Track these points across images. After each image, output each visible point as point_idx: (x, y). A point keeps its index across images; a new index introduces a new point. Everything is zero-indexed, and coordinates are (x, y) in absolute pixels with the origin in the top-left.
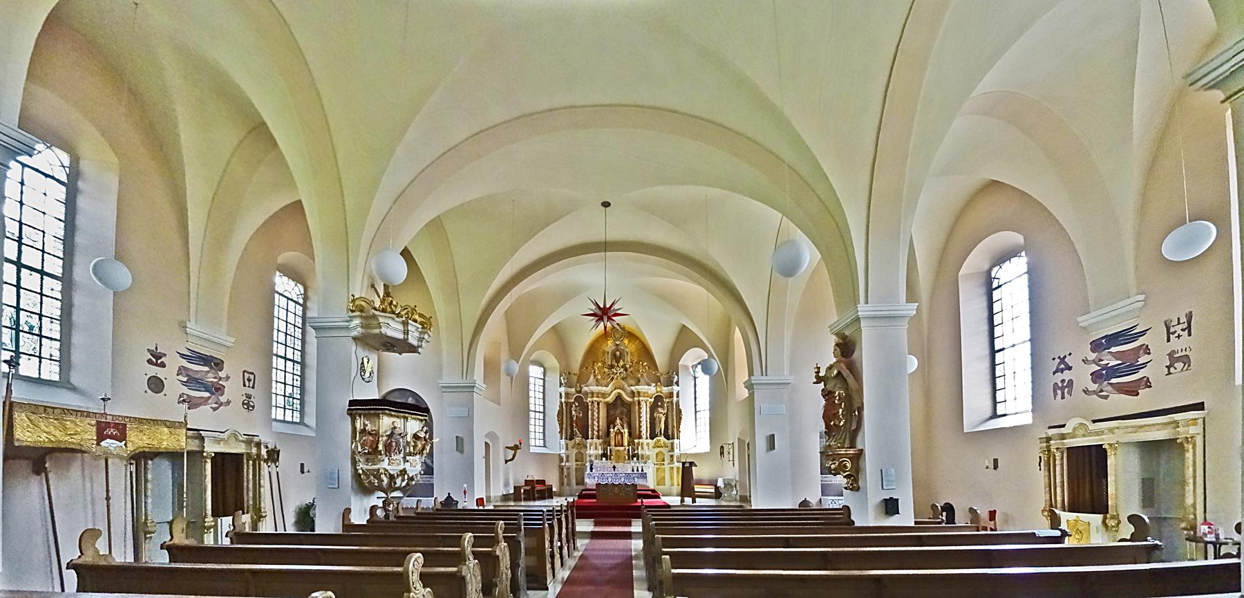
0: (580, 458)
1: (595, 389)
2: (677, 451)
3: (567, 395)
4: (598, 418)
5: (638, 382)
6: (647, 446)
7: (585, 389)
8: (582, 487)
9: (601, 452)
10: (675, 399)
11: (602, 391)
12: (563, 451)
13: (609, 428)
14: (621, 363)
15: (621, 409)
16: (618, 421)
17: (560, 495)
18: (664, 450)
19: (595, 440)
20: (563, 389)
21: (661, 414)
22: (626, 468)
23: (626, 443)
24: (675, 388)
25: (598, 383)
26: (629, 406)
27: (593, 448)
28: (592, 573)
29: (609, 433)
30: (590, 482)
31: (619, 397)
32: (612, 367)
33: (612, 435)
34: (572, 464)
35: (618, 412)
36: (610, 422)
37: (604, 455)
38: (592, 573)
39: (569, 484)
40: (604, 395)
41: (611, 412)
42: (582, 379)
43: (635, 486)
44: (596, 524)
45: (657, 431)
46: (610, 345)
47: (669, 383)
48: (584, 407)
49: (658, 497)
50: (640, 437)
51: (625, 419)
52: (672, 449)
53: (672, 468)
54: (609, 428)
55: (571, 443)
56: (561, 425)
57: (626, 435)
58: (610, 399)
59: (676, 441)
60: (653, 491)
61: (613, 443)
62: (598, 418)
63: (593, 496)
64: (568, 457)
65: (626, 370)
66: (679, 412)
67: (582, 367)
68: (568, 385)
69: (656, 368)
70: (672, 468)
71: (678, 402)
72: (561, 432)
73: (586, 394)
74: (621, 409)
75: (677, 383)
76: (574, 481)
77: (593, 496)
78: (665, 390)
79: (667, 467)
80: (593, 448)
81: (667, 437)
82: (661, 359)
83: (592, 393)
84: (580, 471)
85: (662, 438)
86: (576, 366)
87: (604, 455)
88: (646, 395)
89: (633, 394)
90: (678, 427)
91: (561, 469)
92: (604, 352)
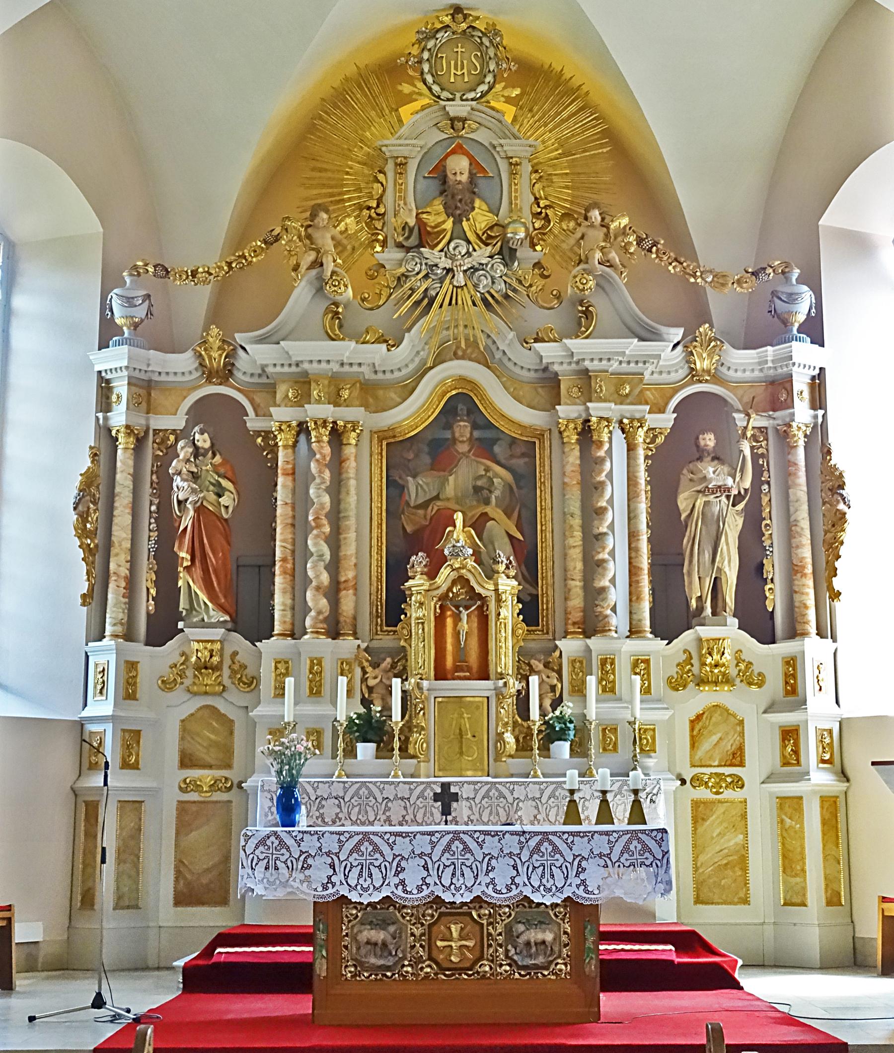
0: (209, 746)
1: (317, 352)
2: (819, 712)
3: (145, 391)
4: (331, 525)
5: (582, 319)
6: (634, 681)
7: (256, 355)
8: (213, 919)
9: (345, 709)
10: (802, 413)
11: (350, 364)
12: (101, 707)
13: (397, 573)
14: (480, 218)
15: (469, 476)
16: (459, 534)
17: (64, 964)
18: (742, 702)
19: (315, 644)
20: (115, 360)
21: (715, 492)
22: (538, 793)
23: (504, 658)
24: (804, 355)
25: (337, 324)
26: (523, 455)
27: (298, 692)
28: (726, 851)
29: (394, 608)
30: (271, 894)
31: (461, 404)
32: (422, 236)
33: (420, 612)
34: (162, 781)
35: (457, 482)
36: (412, 540)
37: (369, 729)
38: (726, 851)
39: (128, 901)
40: (371, 392)
41: (417, 488)
42: (240, 293)
43: (580, 912)
44: (735, 496)
45: (697, 589)
46: (413, 128)
47: (769, 326)
48: (252, 463)
49: (720, 978)
50: (591, 625)
51: (501, 526)
52: (793, 691)
53: (790, 806)
54: (397, 573)
55: (157, 660)
56: (98, 553)
57: (509, 612)
58: (411, 414)
59: (814, 649)
60: (688, 940)
61: (422, 655)
62: (331, 525)
63: (294, 978)
64: (131, 739)
65: (508, 254)
66: (830, 485)
67: (239, 239)
68: (154, 334)
69: (682, 247)
70: (790, 806)
71: (819, 435)
72: (95, 597)
73: (265, 387)
74: (469, 476)
75: (814, 330)
76: (161, 883)
77: (294, 978)
78: (743, 363)
79: (757, 796)
80: (298, 692)
81: (761, 627)
82: (709, 200)
83: (303, 383)
84: (208, 819)
85: (729, 633)
86: (203, 242)
87: (369, 729)
88: (628, 386)
89: (549, 386)
90: (826, 572)
91: (88, 811)
92: (377, 163)
